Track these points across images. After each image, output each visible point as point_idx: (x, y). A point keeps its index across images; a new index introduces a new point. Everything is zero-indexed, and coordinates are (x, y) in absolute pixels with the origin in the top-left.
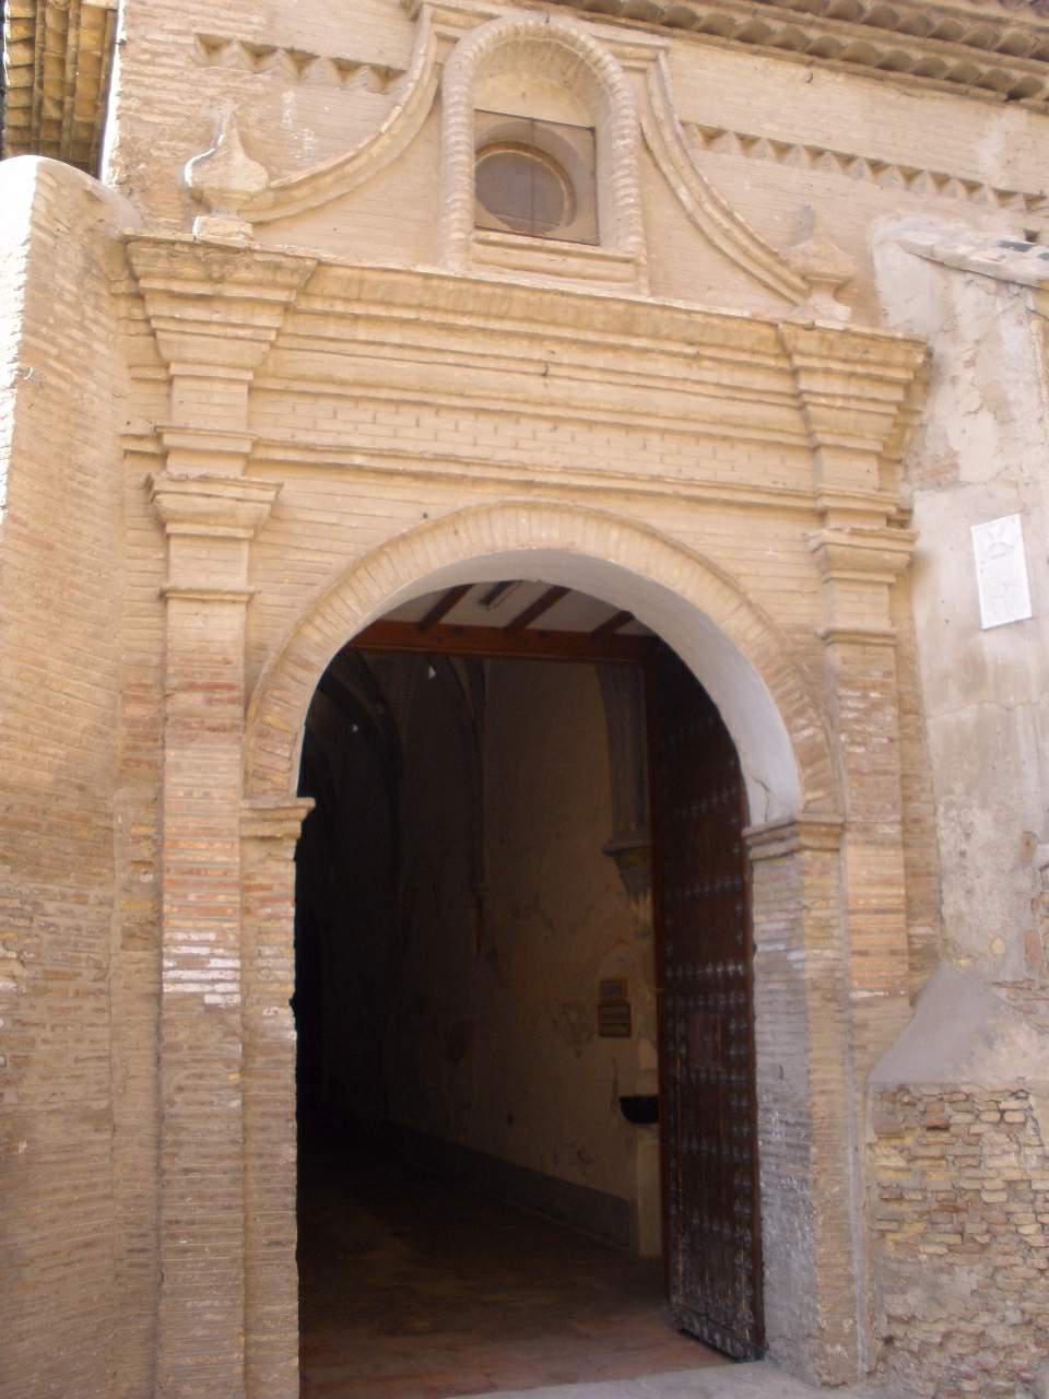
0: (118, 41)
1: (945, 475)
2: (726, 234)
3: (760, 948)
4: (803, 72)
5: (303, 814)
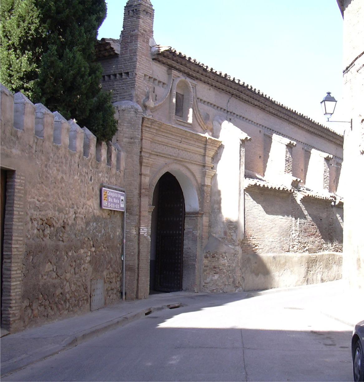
2: (201, 122)
3: (186, 230)
5: (153, 208)
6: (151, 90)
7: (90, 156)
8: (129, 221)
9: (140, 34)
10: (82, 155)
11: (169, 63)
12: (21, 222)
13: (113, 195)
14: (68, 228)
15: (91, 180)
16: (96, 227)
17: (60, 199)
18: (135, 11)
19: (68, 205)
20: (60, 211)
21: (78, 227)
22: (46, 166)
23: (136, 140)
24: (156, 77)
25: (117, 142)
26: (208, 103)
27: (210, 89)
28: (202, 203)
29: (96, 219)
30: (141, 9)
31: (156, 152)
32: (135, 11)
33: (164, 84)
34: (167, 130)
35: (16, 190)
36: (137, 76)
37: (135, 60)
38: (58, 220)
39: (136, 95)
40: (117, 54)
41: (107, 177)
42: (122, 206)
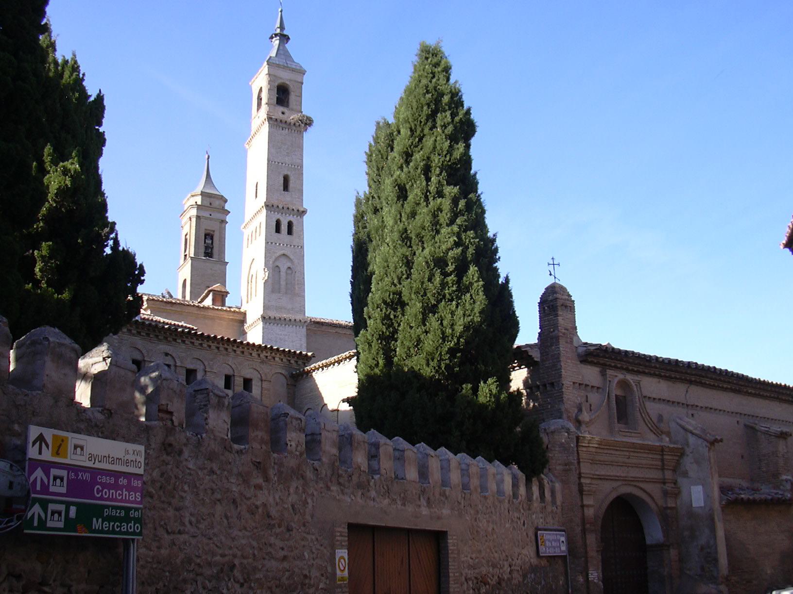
0: (27, 459)
1: (685, 474)
4: (658, 380)
6: (584, 399)
7: (520, 498)
8: (572, 566)
9: (561, 334)
10: (512, 498)
11: (602, 362)
12: (457, 583)
13: (551, 538)
14: (504, 584)
15: (524, 524)
16: (534, 579)
17: (493, 553)
18: (551, 307)
19: (502, 558)
20: (494, 566)
21: (515, 582)
22: (476, 520)
23: (571, 467)
24: (588, 383)
25: (549, 472)
26: (660, 399)
27: (659, 382)
28: (666, 533)
29: (534, 569)
30: (559, 303)
31: (598, 475)
32: (551, 307)
33: (598, 388)
34: (609, 446)
35: (450, 552)
36: (564, 386)
37: (559, 367)
38: (493, 576)
39: (566, 410)
40: (536, 362)
41: (541, 518)
42: (564, 548)
